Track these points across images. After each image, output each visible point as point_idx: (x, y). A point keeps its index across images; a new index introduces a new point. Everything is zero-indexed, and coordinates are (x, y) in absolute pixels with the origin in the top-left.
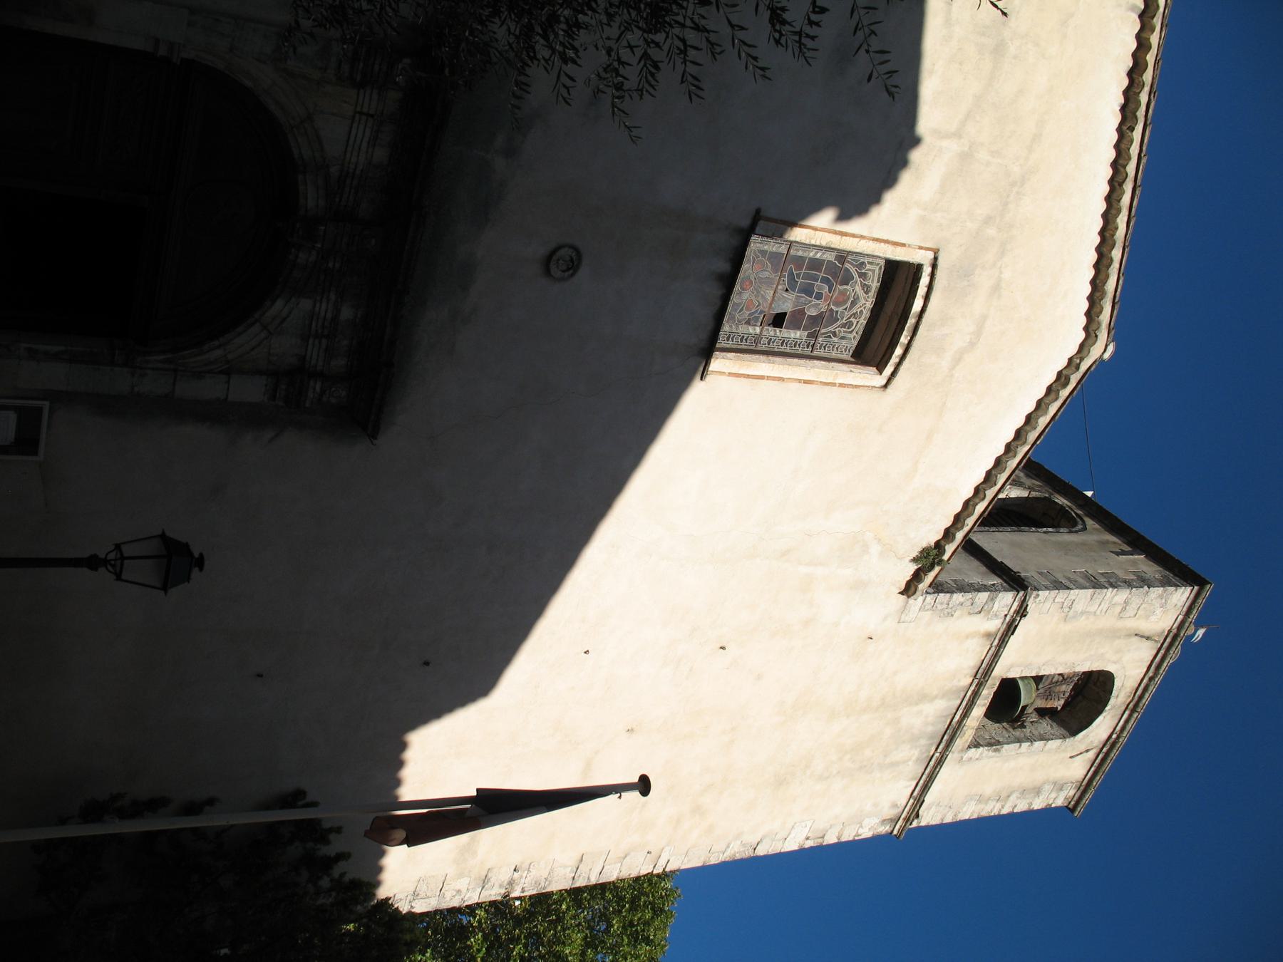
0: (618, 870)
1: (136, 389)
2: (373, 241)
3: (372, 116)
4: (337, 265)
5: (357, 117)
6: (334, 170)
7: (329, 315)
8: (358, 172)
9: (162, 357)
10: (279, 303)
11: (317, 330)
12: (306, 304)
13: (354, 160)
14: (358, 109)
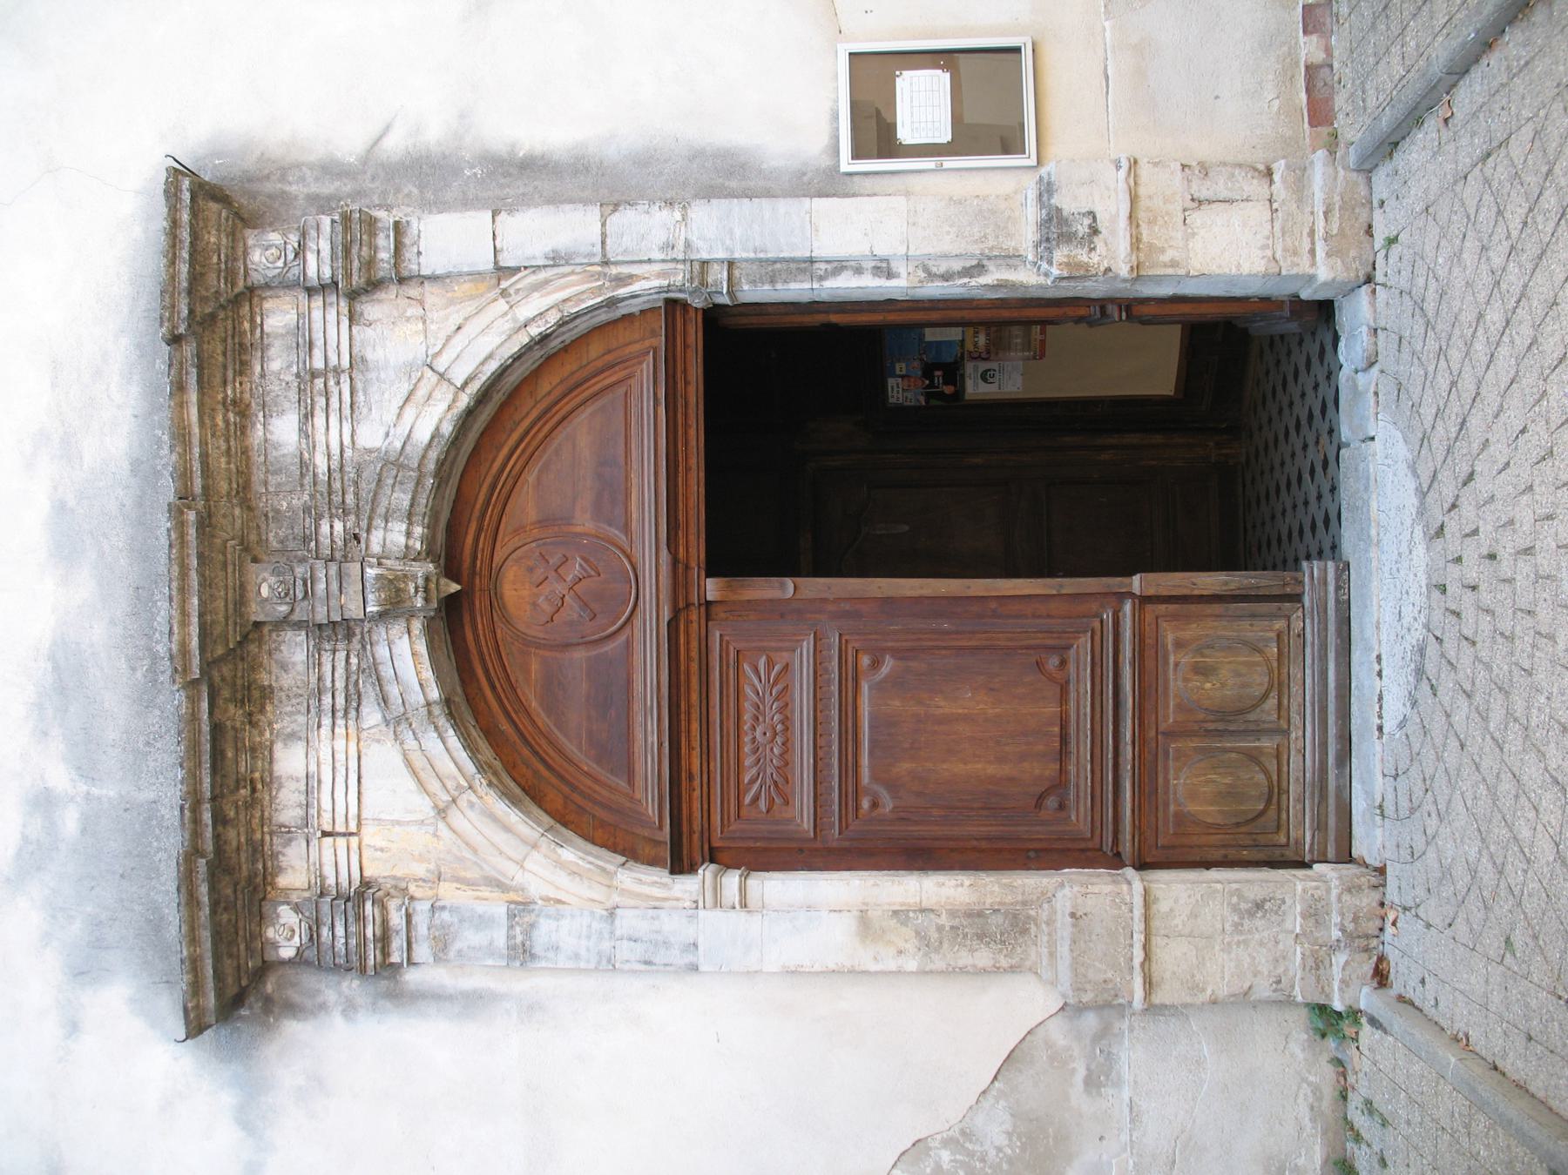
0: (1420, 782)
1: (678, 215)
2: (265, 591)
3: (325, 834)
4: (325, 528)
5: (353, 827)
6: (372, 715)
7: (319, 420)
8: (327, 721)
9: (636, 287)
10: (423, 435)
11: (338, 383)
12: (371, 436)
13: (340, 744)
14: (354, 841)
